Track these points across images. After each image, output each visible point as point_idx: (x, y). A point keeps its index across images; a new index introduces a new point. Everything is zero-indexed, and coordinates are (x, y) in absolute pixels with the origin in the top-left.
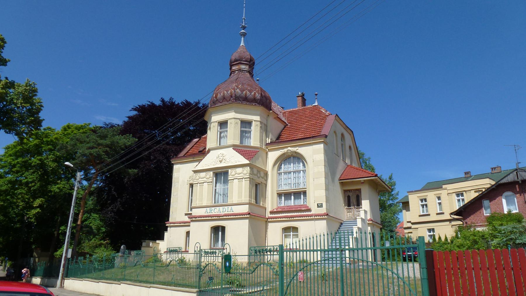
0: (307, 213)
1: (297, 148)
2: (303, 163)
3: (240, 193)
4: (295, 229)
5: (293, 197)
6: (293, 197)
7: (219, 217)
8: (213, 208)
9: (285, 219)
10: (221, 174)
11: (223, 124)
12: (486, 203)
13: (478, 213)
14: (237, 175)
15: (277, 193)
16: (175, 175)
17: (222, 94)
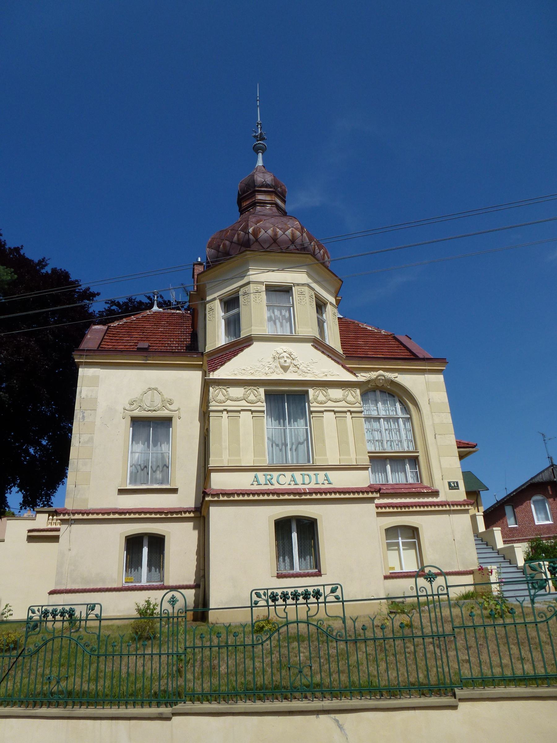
0: (430, 500)
2: (402, 403)
4: (413, 532)
5: (388, 467)
6: (388, 467)
7: (299, 496)
8: (275, 474)
9: (391, 510)
10: (287, 399)
12: (508, 510)
17: (270, 231)
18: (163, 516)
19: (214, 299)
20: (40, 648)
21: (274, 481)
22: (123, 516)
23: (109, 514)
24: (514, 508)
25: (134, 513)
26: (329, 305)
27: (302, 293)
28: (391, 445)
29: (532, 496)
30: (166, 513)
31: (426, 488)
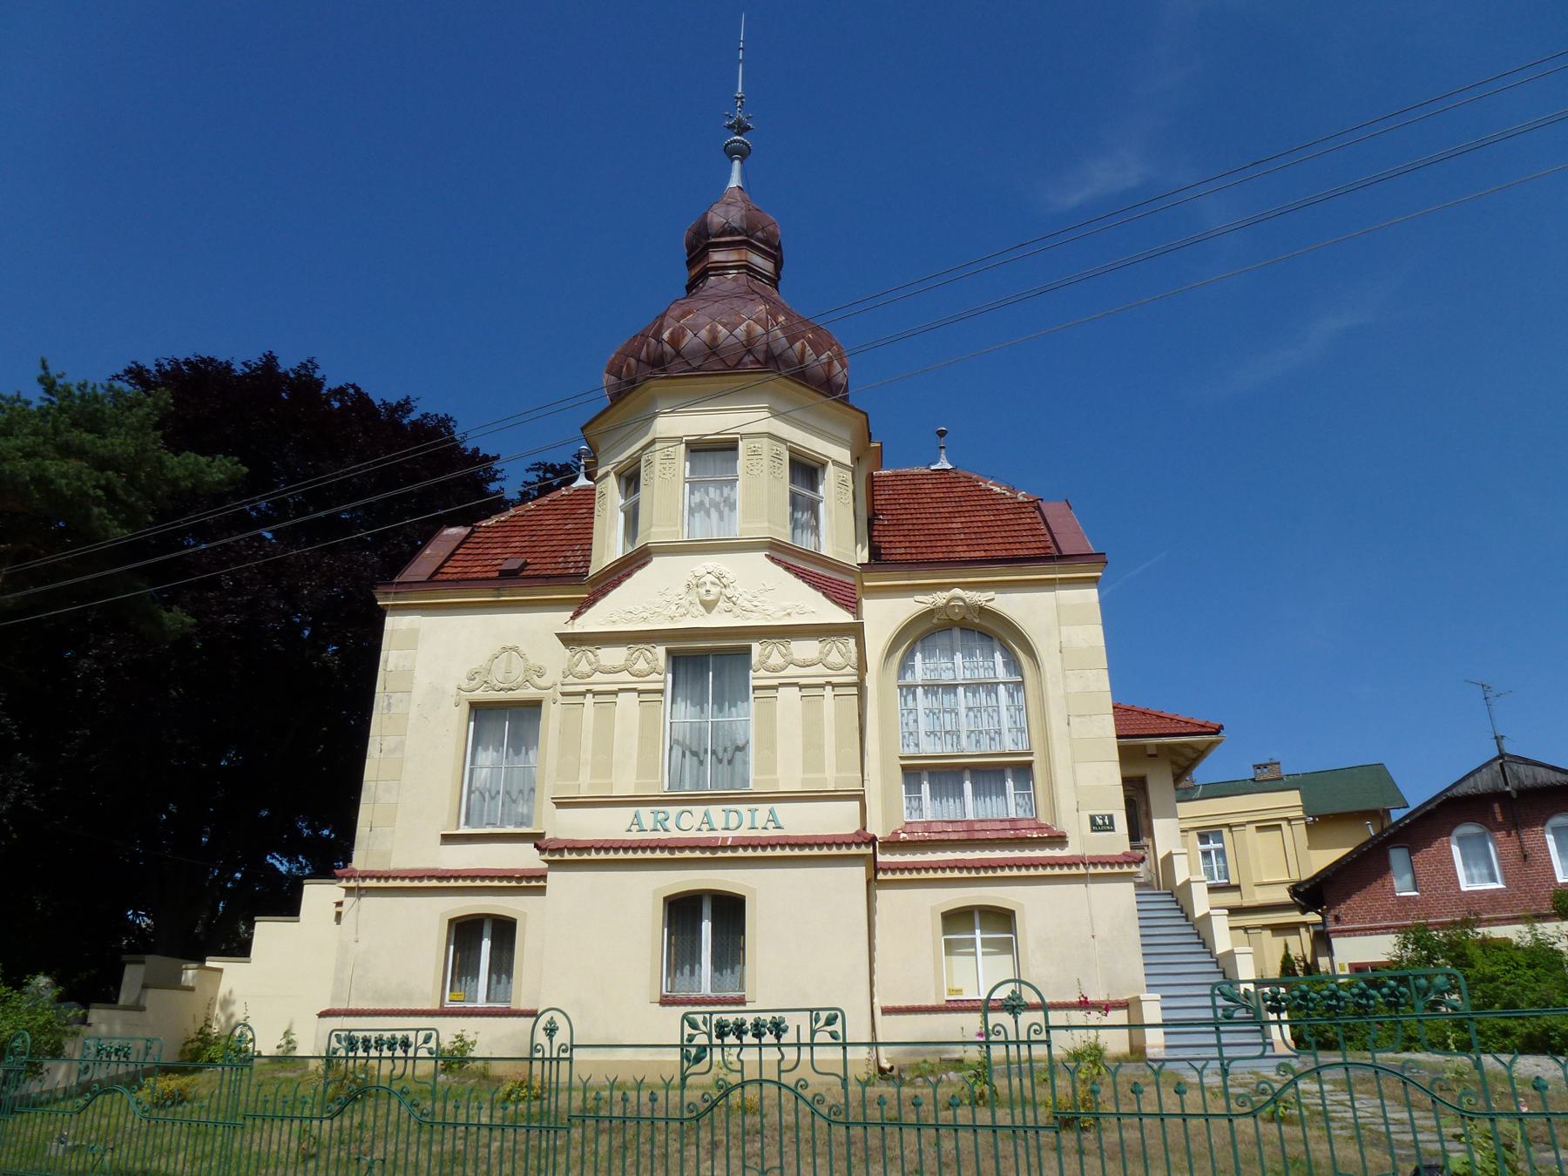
0: (1048, 853)
1: (991, 594)
3: (812, 746)
4: (1002, 918)
5: (968, 786)
6: (968, 786)
7: (712, 853)
8: (673, 811)
10: (707, 662)
11: (713, 452)
12: (1397, 857)
13: (1376, 885)
14: (792, 670)
15: (904, 768)
16: (391, 657)
17: (704, 333)
18: (514, 884)
19: (606, 475)
20: (714, 1104)
21: (670, 824)
22: (445, 884)
23: (421, 878)
24: (1412, 852)
25: (465, 878)
26: (830, 468)
27: (755, 452)
28: (978, 741)
29: (1455, 825)
30: (520, 879)
31: (1040, 828)
